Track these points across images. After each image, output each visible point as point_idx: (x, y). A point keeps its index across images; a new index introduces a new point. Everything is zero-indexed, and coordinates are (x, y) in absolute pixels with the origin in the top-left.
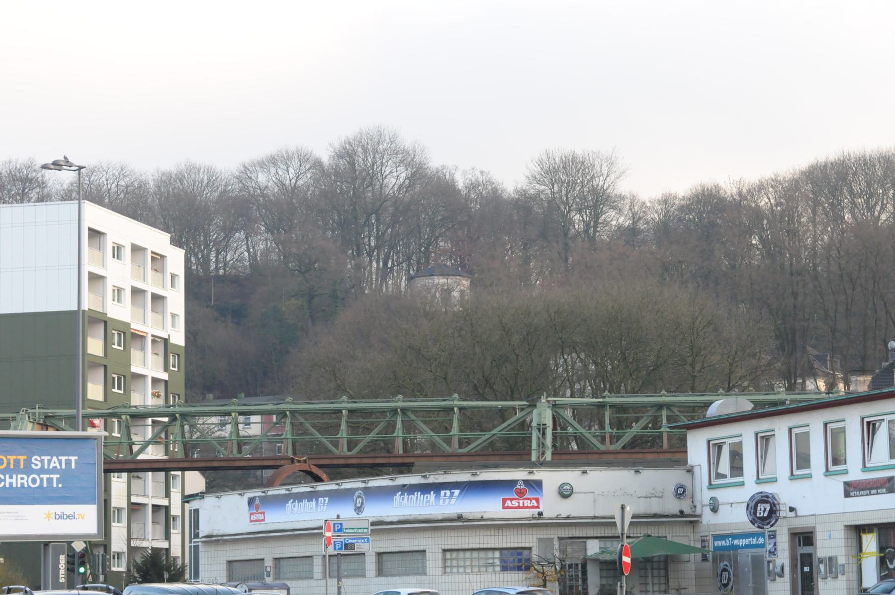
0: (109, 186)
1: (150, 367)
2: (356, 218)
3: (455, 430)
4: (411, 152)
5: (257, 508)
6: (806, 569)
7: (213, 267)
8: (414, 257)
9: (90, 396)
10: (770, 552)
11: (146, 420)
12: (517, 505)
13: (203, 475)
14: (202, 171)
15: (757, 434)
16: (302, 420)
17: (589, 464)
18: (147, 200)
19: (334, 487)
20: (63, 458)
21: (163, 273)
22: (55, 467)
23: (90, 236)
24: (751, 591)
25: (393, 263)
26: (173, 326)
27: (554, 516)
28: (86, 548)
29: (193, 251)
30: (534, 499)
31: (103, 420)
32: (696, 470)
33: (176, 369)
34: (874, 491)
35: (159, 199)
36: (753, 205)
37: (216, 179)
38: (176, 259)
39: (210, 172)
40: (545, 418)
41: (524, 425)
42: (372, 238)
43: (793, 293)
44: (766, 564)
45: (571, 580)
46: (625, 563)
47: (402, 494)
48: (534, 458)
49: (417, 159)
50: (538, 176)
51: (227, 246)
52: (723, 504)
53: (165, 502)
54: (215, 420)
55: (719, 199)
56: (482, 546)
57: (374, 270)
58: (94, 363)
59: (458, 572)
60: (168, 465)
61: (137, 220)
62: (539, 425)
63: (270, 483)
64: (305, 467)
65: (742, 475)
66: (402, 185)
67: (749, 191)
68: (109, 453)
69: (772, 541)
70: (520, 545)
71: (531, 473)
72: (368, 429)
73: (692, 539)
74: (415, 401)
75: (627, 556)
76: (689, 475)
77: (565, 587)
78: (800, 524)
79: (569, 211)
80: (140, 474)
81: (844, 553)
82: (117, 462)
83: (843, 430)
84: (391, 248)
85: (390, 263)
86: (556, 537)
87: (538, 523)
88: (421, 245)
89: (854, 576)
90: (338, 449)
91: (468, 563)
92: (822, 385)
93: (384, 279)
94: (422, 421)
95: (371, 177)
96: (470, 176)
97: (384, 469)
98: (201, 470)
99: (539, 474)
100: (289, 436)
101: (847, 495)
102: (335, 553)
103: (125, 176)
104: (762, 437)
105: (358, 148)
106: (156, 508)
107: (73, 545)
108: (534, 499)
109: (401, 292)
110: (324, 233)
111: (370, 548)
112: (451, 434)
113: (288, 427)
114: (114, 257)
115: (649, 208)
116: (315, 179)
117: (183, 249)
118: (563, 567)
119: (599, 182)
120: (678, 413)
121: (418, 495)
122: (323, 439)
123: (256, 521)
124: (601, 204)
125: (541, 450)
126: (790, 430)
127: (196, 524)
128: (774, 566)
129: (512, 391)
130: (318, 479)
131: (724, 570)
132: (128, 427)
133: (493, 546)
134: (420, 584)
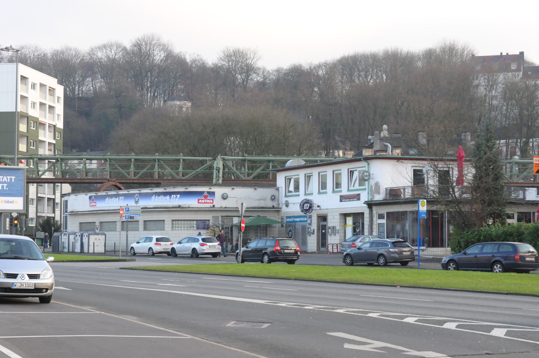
1: (47, 138)
2: (141, 74)
3: (181, 169)
4: (167, 45)
6: (323, 231)
8: (167, 92)
9: (20, 149)
10: (309, 224)
12: (204, 202)
13: (70, 185)
14: (72, 50)
15: (305, 175)
16: (114, 163)
18: (47, 62)
19: (126, 192)
20: (9, 177)
21: (54, 96)
22: (5, 181)
23: (21, 79)
25: (157, 94)
26: (58, 119)
27: (220, 207)
28: (18, 216)
29: (68, 86)
30: (211, 199)
31: (26, 160)
32: (280, 189)
33: (59, 139)
34: (352, 200)
35: (53, 62)
38: (60, 90)
39: (76, 51)
40: (219, 165)
41: (211, 167)
42: (148, 83)
43: (330, 113)
44: (307, 229)
47: (155, 196)
48: (214, 182)
49: (169, 48)
50: (222, 58)
51: (83, 84)
52: (290, 204)
53: (53, 197)
54: (76, 161)
55: (301, 70)
57: (149, 97)
58: (22, 135)
59: (178, 230)
60: (54, 181)
61: (43, 73)
62: (217, 168)
63: (98, 190)
64: (114, 183)
66: (162, 59)
67: (314, 68)
69: (310, 219)
70: (205, 219)
71: (210, 188)
72: (143, 167)
73: (277, 218)
74: (164, 156)
75: (243, 223)
76: (277, 191)
78: (321, 212)
79: (236, 74)
80: (42, 184)
81: (339, 225)
82: (32, 179)
83: (340, 174)
84: (157, 87)
85: (156, 94)
86: (220, 216)
87: (212, 210)
88: (170, 87)
91: (182, 226)
93: (153, 101)
94: (166, 165)
95: (148, 55)
96: (192, 57)
97: (150, 185)
98: (70, 183)
99: (213, 189)
101: (341, 201)
102: (126, 220)
104: (308, 176)
105: (143, 42)
106: (49, 199)
107: (12, 214)
108: (211, 199)
109: (160, 107)
110: (127, 79)
111: (141, 218)
112: (179, 171)
113: (108, 166)
114: (32, 88)
115: (271, 73)
116: (123, 56)
119: (249, 61)
120: (277, 164)
121: (162, 197)
122: (123, 172)
124: (250, 71)
125: (217, 179)
126: (319, 173)
127: (66, 206)
128: (311, 230)
130: (120, 189)
131: (290, 231)
132: (37, 164)
133: (193, 219)
134: (162, 234)
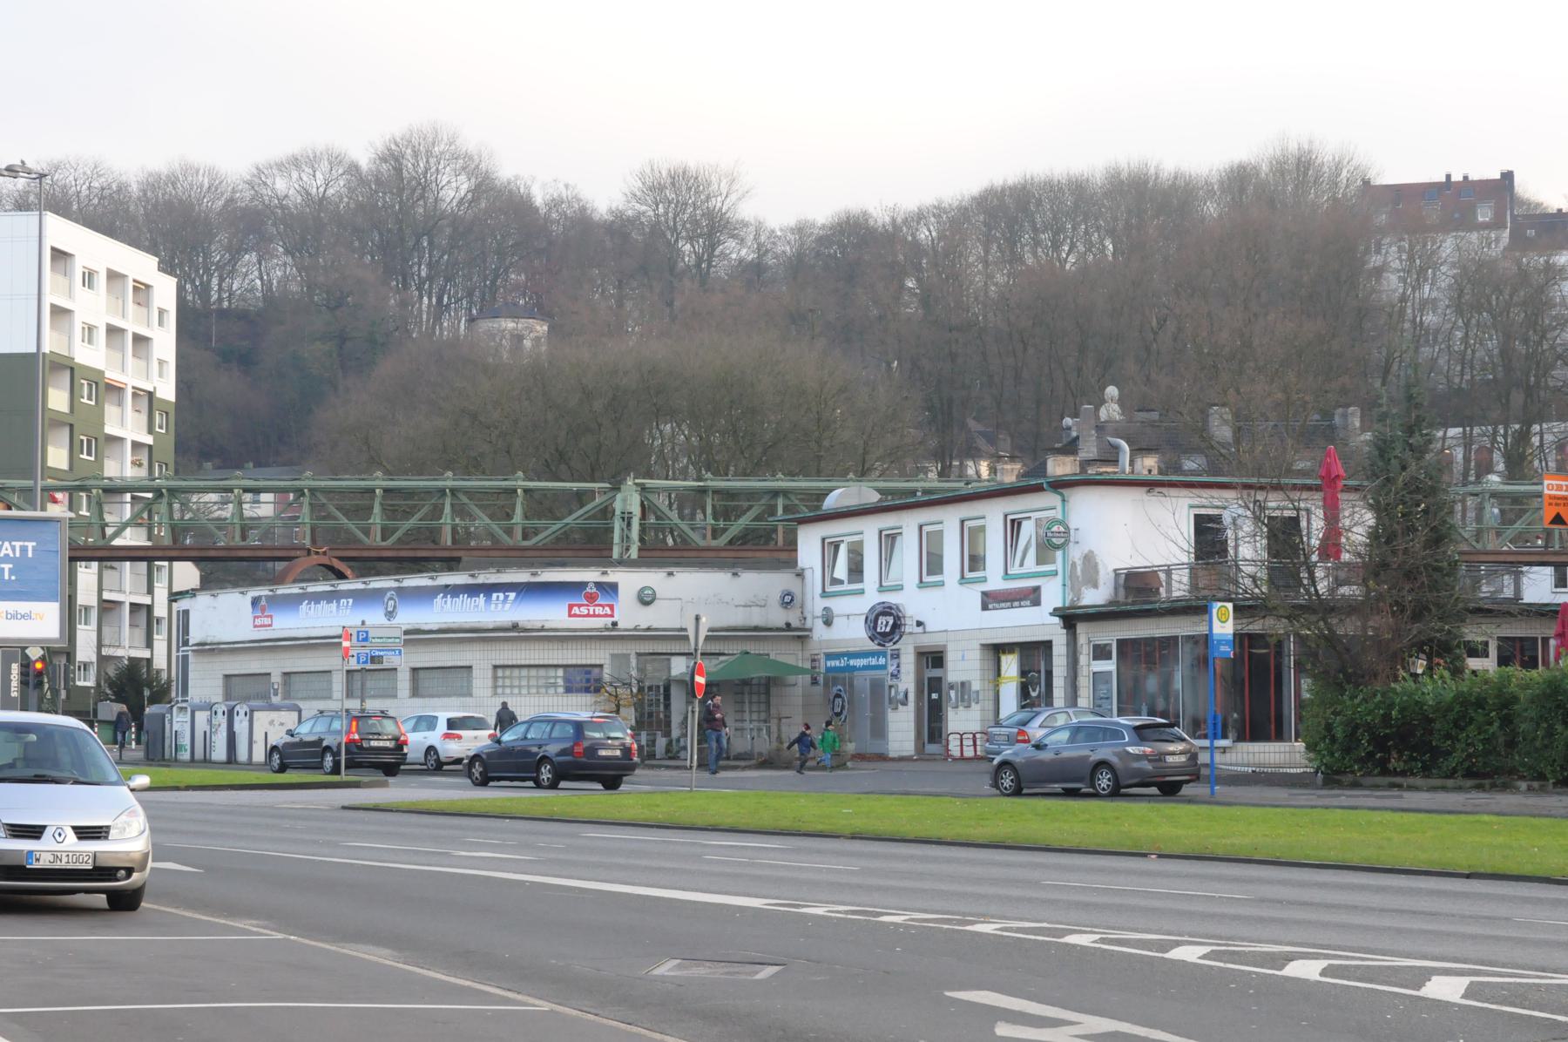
0: (78, 188)
2: (402, 240)
3: (518, 517)
5: (263, 610)
6: (934, 696)
7: (215, 297)
8: (477, 293)
9: (51, 463)
10: (892, 675)
11: (124, 495)
12: (586, 612)
13: (197, 566)
14: (201, 172)
15: (881, 532)
17: (678, 564)
19: (360, 586)
20: (18, 544)
23: (54, 258)
24: (869, 722)
25: (449, 298)
26: (161, 375)
27: (632, 627)
31: (67, 495)
32: (808, 574)
33: (163, 431)
34: (1016, 604)
36: (910, 238)
37: (221, 183)
38: (165, 290)
40: (631, 505)
41: (606, 512)
44: (887, 688)
45: (651, 705)
46: (698, 683)
49: (483, 166)
50: (638, 194)
52: (838, 616)
53: (146, 600)
54: (214, 497)
55: (867, 228)
56: (541, 663)
57: (424, 307)
58: (57, 421)
60: (150, 554)
63: (279, 580)
64: (325, 560)
65: (862, 581)
66: (462, 199)
67: (905, 221)
68: (75, 537)
69: (895, 662)
70: (589, 662)
71: (604, 573)
74: (468, 480)
75: (701, 675)
76: (798, 581)
77: (642, 715)
78: (928, 641)
80: (115, 564)
82: (86, 548)
83: (982, 529)
85: (446, 299)
87: (611, 635)
89: (990, 706)
90: (369, 538)
91: (524, 683)
92: (984, 468)
93: (438, 319)
95: (424, 187)
96: (551, 191)
99: (614, 576)
100: (307, 520)
101: (985, 607)
102: (359, 668)
103: (99, 176)
106: (135, 607)
107: (27, 651)
109: (459, 336)
111: (404, 661)
113: (306, 509)
114: (84, 285)
115: (779, 238)
116: (349, 189)
117: (175, 276)
118: (641, 689)
119: (716, 203)
120: (797, 502)
121: (464, 598)
122: (350, 525)
123: (261, 626)
125: (625, 545)
127: (185, 629)
128: (897, 692)
129: (593, 470)
130: (341, 576)
131: (838, 696)
132: (100, 505)
133: (555, 662)
134: (464, 707)
